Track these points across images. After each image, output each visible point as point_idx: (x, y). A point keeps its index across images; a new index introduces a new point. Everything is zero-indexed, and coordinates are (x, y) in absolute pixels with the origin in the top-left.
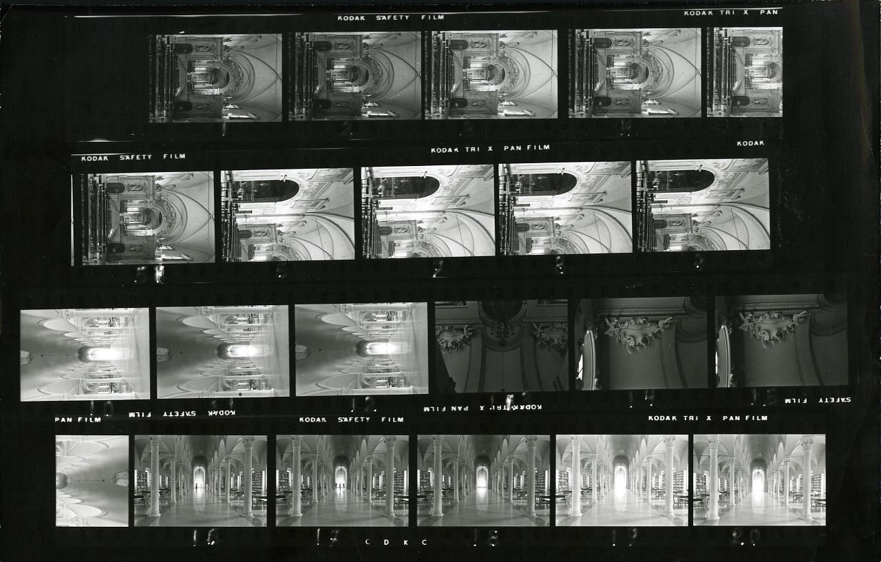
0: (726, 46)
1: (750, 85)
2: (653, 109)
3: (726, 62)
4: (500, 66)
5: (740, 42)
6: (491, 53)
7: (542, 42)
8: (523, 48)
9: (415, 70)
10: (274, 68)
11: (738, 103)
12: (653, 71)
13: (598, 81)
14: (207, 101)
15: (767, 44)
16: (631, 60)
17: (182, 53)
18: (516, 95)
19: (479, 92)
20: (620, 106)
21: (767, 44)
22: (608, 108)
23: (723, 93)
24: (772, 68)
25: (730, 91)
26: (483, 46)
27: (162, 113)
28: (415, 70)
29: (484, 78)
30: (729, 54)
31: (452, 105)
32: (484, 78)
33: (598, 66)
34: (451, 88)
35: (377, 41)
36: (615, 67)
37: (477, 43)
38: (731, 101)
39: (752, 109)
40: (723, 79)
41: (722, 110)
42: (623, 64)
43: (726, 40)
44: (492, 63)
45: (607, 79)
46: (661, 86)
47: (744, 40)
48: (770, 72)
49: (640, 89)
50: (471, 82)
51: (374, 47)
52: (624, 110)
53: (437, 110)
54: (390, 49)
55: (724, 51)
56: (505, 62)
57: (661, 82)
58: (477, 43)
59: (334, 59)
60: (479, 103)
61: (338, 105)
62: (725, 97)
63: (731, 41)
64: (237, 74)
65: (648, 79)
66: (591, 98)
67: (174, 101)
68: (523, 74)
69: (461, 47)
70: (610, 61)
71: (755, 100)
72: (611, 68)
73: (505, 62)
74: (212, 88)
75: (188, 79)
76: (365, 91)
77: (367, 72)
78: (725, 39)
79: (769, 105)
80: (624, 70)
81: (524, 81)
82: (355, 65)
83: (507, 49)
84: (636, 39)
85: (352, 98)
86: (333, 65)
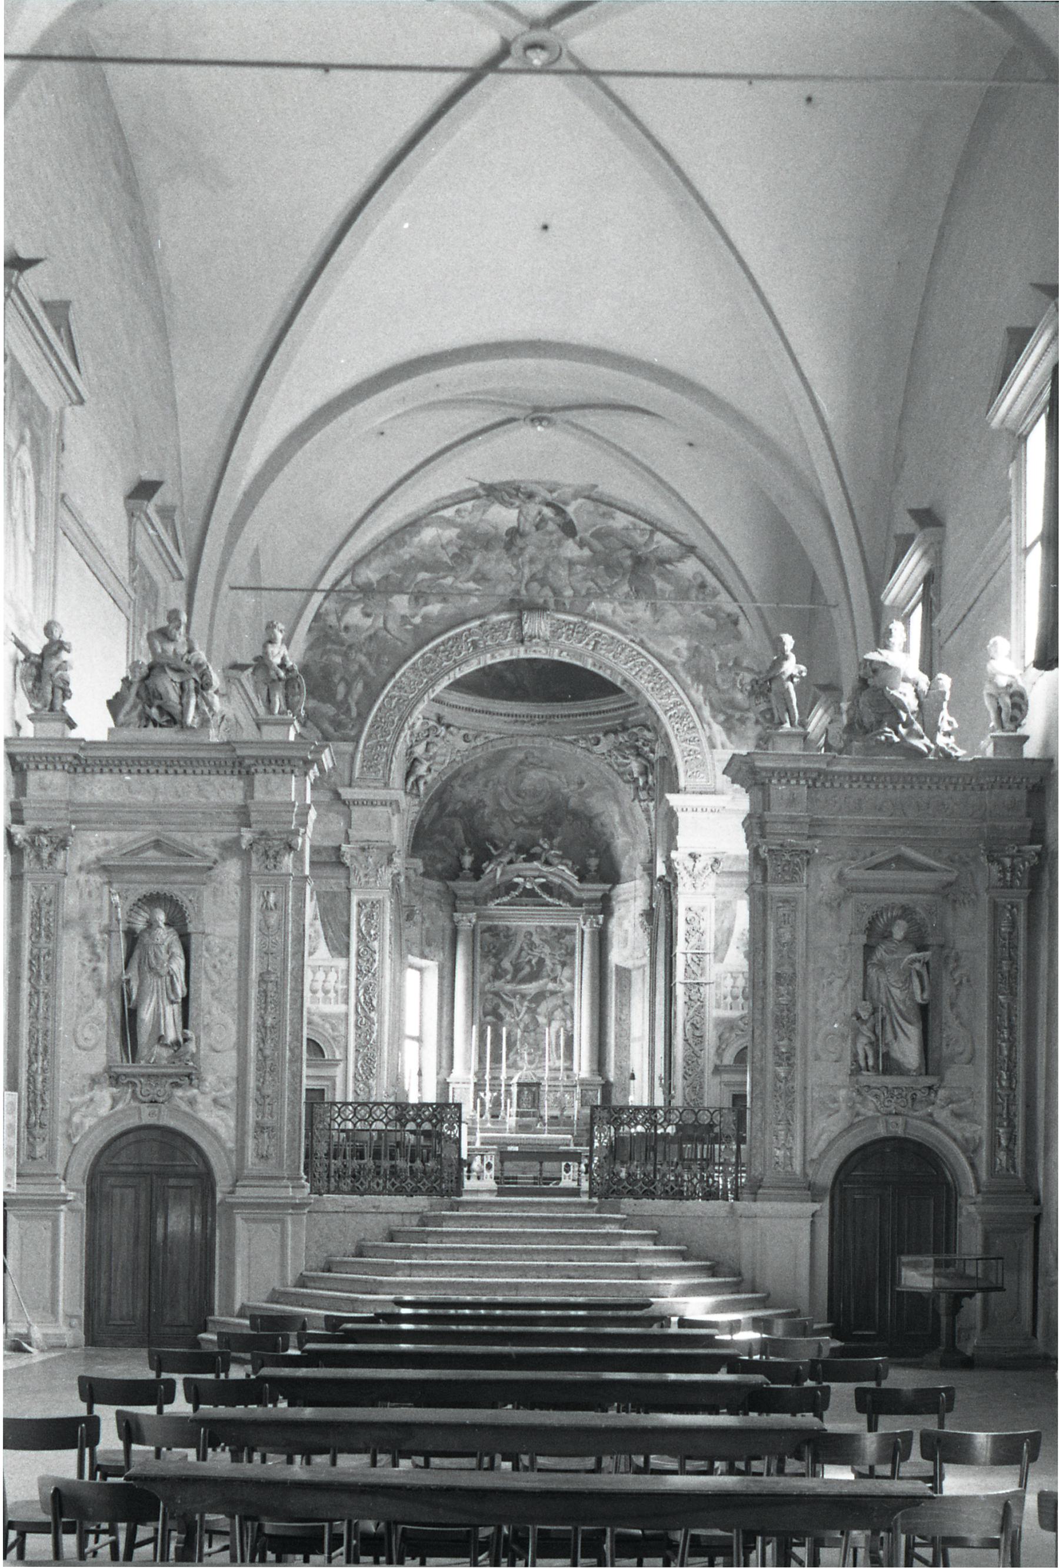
0: (207, 1434)
1: (697, 1132)
2: (991, 608)
3: (397, 1441)
4: (431, 725)
5: (152, 1252)
6: (264, 844)
7: (131, 185)
8: (197, 438)
9: (475, 76)
10: (424, 94)
11: (917, 1278)
12: (521, 607)
13: (638, 1310)
14: (829, 943)
15: (178, 921)
16: (374, 890)
17: (203, 1259)
18: (817, 548)
19: (755, 984)
20: (951, 1030)
21: (178, 921)
22: (969, 1178)
23: (793, 1480)
24: (484, 852)
25: (772, 1385)
26: (165, 935)
27: (981, 1525)
28: (475, 76)
29: (584, 927)
30: (299, 1392)
31: (920, 1330)
32: (584, 927)
33: (439, 1315)
34: (696, 1347)
35: (90, 549)
36: (463, 1093)
37: (128, 1022)
38: (902, 1379)
39: (1001, 1110)
40: (617, 1478)
41: (1001, 1483)
42: (417, 991)
43: (130, 1431)
44: (389, 820)
45: (608, 1190)
46: (706, 500)
47: (124, 1201)
48: (529, 873)
49: (743, 772)
50: (638, 1095)
51: (174, 596)
52: (1003, 979)
53: (985, 1525)
54: (207, 383)
55: (273, 1466)
56: (387, 655)
57: (661, 509)
58: (128, 1022)
59: (316, 1097)
60: (899, 992)
61: (907, 1049)
62: (840, 1449)
63: (135, 1368)
64: (498, 564)
65: (615, 666)
66: (842, 1392)
67: (827, 1370)
68: (531, 438)
69: (178, 1221)
70: (384, 1149)
71: (889, 1066)
72: (471, 1137)
73: (387, 655)
74: (665, 890)
75: (545, 1185)
76: (731, 718)
77: (497, 683)
78: (110, 1441)
79: (948, 893)
80: (503, 983)
81: (631, 430)
82: (397, 832)
83: (213, 641)
84: (108, 815)
85: (823, 879)
86: (402, 1110)
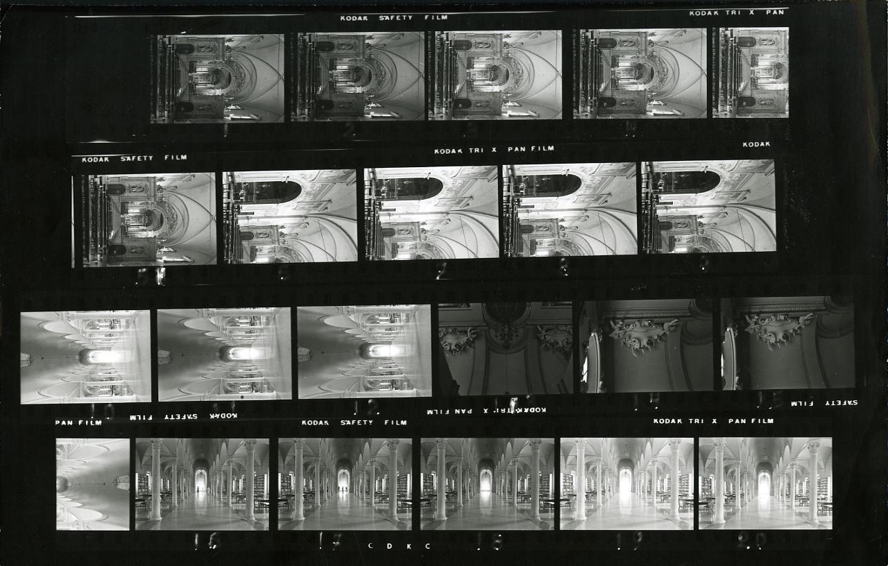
0: (732, 46)
1: (756, 86)
2: (658, 109)
3: (731, 62)
4: (504, 67)
5: (746, 42)
6: (494, 54)
7: (546, 43)
8: (527, 48)
9: (418, 71)
10: (276, 69)
11: (744, 103)
12: (658, 72)
13: (602, 82)
14: (209, 102)
15: (773, 44)
16: (636, 60)
17: (184, 53)
18: (520, 96)
19: (483, 92)
20: (625, 107)
21: (773, 44)
22: (613, 108)
23: (728, 94)
24: (778, 68)
25: (736, 92)
26: (487, 46)
27: (163, 114)
28: (418, 71)
29: (488, 79)
30: (735, 54)
31: (456, 106)
32: (488, 79)
33: (602, 66)
34: (455, 88)
35: (380, 41)
36: (620, 68)
37: (480, 43)
38: (736, 102)
39: (758, 110)
40: (728, 79)
41: (728, 110)
42: (628, 64)
43: (732, 41)
44: (496, 63)
45: (612, 79)
46: (667, 87)
47: (750, 40)
48: (776, 72)
49: (645, 90)
50: (475, 83)
51: (377, 47)
52: (629, 111)
53: (441, 111)
54: (393, 49)
55: (729, 52)
56: (509, 63)
57: (666, 83)
58: (480, 43)
59: (337, 59)
60: (483, 104)
61: (341, 106)
62: (731, 97)
63: (737, 41)
64: (239, 75)
65: (653, 80)
66: (596, 98)
67: (175, 102)
68: (527, 75)
69: (464, 47)
70: (615, 62)
71: (761, 101)
72: (616, 68)
73: (509, 63)
74: (213, 89)
75: (190, 79)
76: (367, 91)
77: (370, 73)
78: (731, 39)
79: (775, 106)
80: (629, 71)
81: (528, 82)
82: (358, 65)
83: (511, 49)
84: (641, 40)
85: (354, 98)
86: (336, 66)
